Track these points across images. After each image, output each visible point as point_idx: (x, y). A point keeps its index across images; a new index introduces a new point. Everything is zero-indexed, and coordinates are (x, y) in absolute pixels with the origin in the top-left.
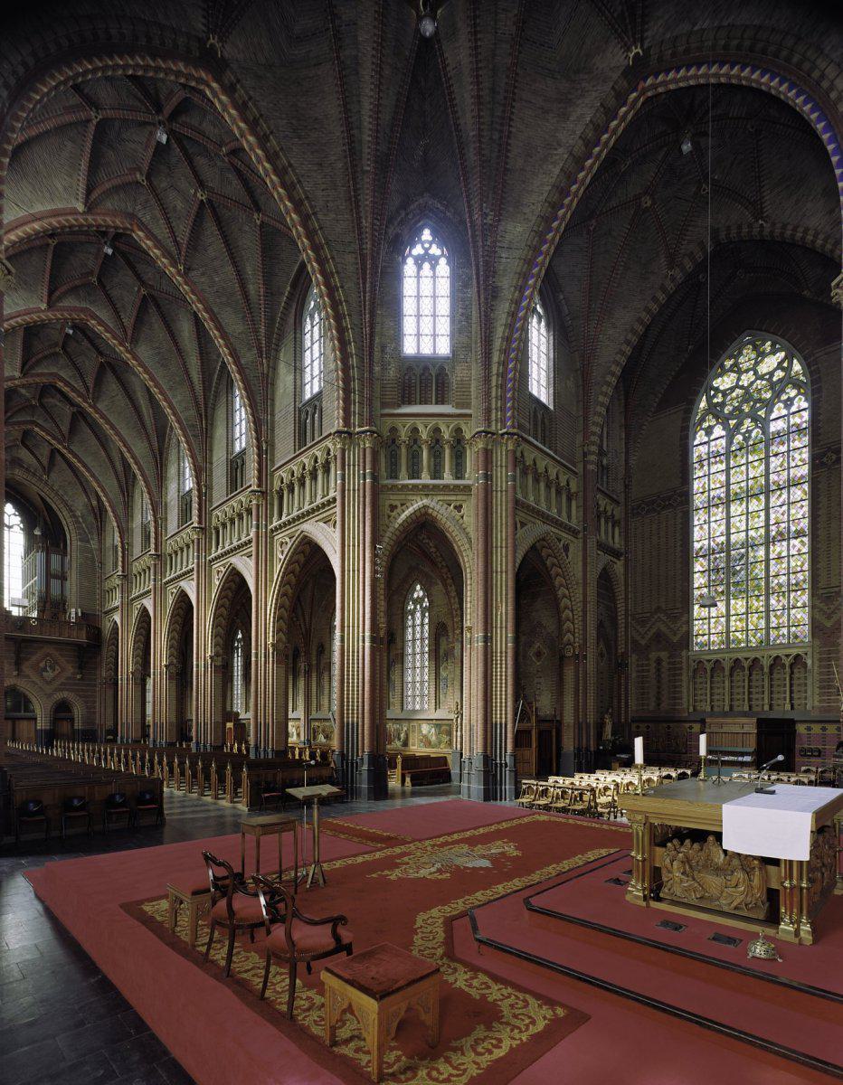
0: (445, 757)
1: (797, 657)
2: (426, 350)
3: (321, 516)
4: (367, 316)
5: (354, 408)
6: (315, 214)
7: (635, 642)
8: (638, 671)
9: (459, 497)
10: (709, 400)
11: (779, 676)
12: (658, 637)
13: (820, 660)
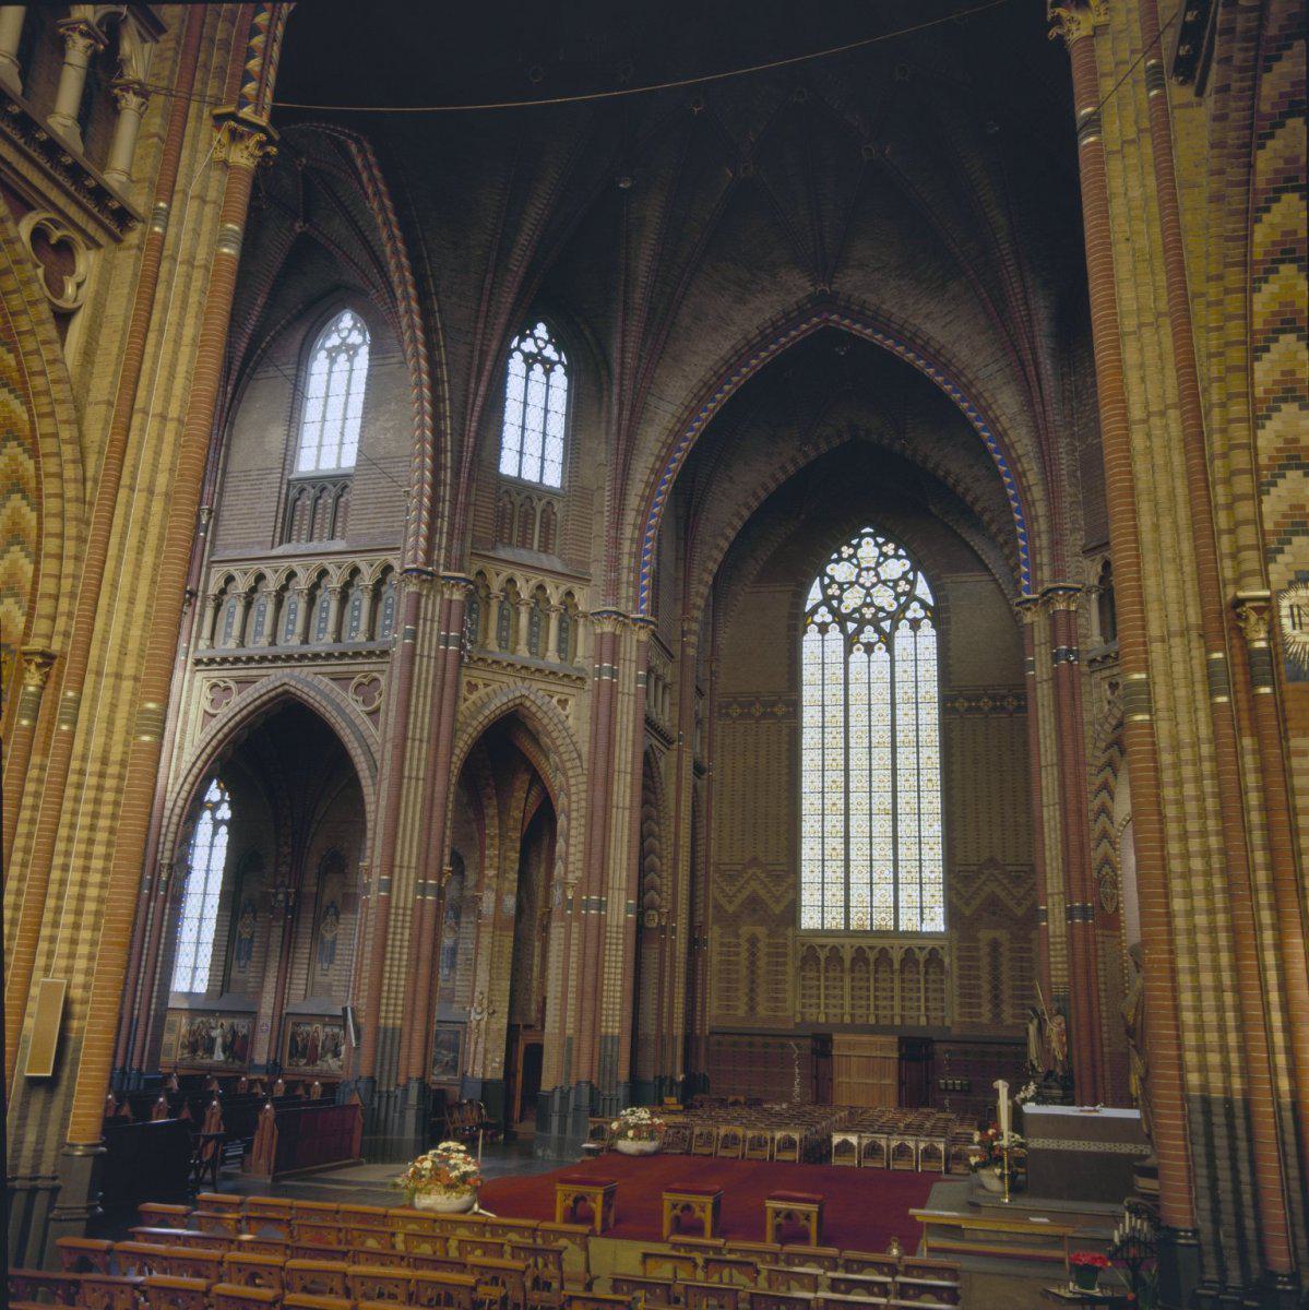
0: (443, 1091)
1: (933, 951)
2: (531, 474)
3: (329, 669)
4: (474, 424)
5: (441, 539)
6: (436, 294)
7: (718, 907)
8: (721, 954)
9: (566, 690)
10: (824, 588)
11: (910, 976)
12: (754, 903)
13: (960, 958)
